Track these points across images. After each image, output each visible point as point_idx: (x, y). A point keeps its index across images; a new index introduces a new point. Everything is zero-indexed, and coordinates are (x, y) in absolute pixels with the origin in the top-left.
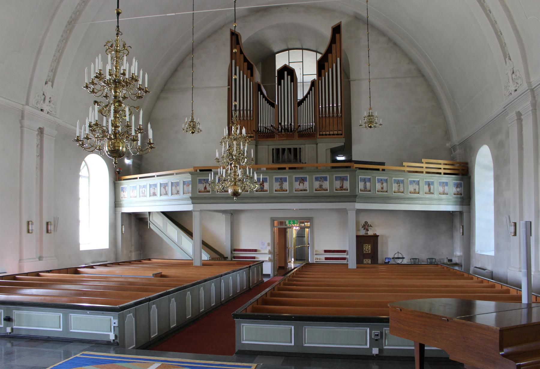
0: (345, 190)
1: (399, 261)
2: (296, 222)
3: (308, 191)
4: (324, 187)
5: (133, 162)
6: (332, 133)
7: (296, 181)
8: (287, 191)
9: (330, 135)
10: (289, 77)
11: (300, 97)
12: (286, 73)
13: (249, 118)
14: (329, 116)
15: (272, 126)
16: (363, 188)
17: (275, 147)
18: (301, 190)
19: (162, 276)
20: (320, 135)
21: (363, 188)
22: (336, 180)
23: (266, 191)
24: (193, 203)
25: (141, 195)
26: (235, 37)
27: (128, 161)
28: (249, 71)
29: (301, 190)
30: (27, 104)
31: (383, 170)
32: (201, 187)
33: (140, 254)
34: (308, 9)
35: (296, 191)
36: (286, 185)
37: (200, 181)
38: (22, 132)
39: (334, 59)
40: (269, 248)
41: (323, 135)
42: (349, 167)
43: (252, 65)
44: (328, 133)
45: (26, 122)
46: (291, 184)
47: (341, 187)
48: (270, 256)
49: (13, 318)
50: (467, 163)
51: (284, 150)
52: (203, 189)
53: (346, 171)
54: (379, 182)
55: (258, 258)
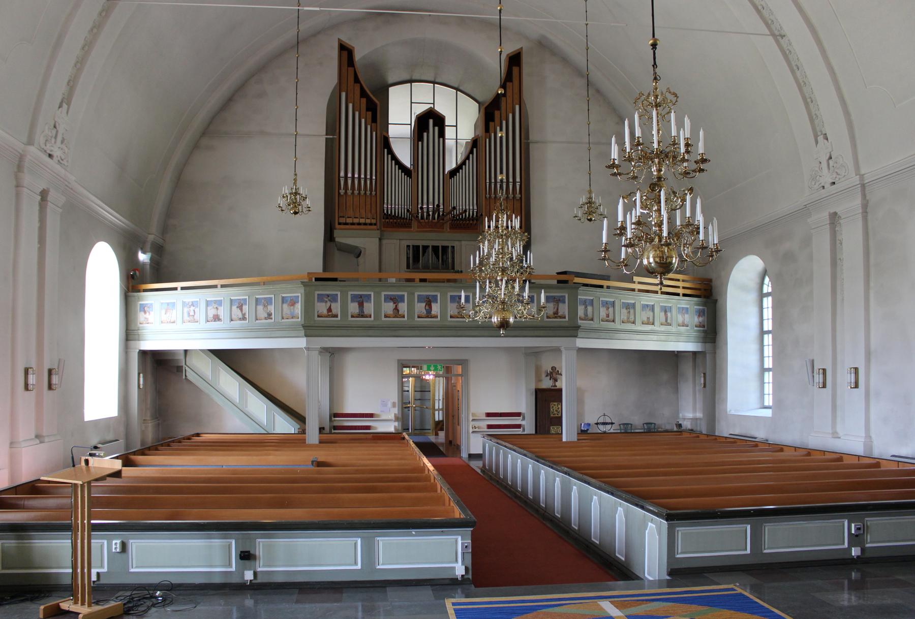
0: (561, 317)
1: (607, 428)
2: (439, 367)
5: (151, 259)
10: (436, 128)
11: (451, 165)
12: (431, 121)
13: (368, 193)
16: (583, 316)
17: (411, 243)
19: (320, 464)
20: (340, 224)
21: (583, 316)
22: (352, 301)
23: (436, 317)
24: (306, 336)
25: (186, 317)
26: (346, 52)
27: (143, 257)
28: (370, 113)
30: (30, 142)
31: (608, 287)
32: (322, 308)
33: (159, 424)
35: (319, 316)
37: (321, 298)
38: (18, 195)
40: (395, 411)
43: (376, 105)
45: (27, 179)
48: (396, 424)
49: (257, 554)
50: (710, 281)
51: (425, 248)
52: (325, 312)
54: (603, 306)
55: (375, 428)
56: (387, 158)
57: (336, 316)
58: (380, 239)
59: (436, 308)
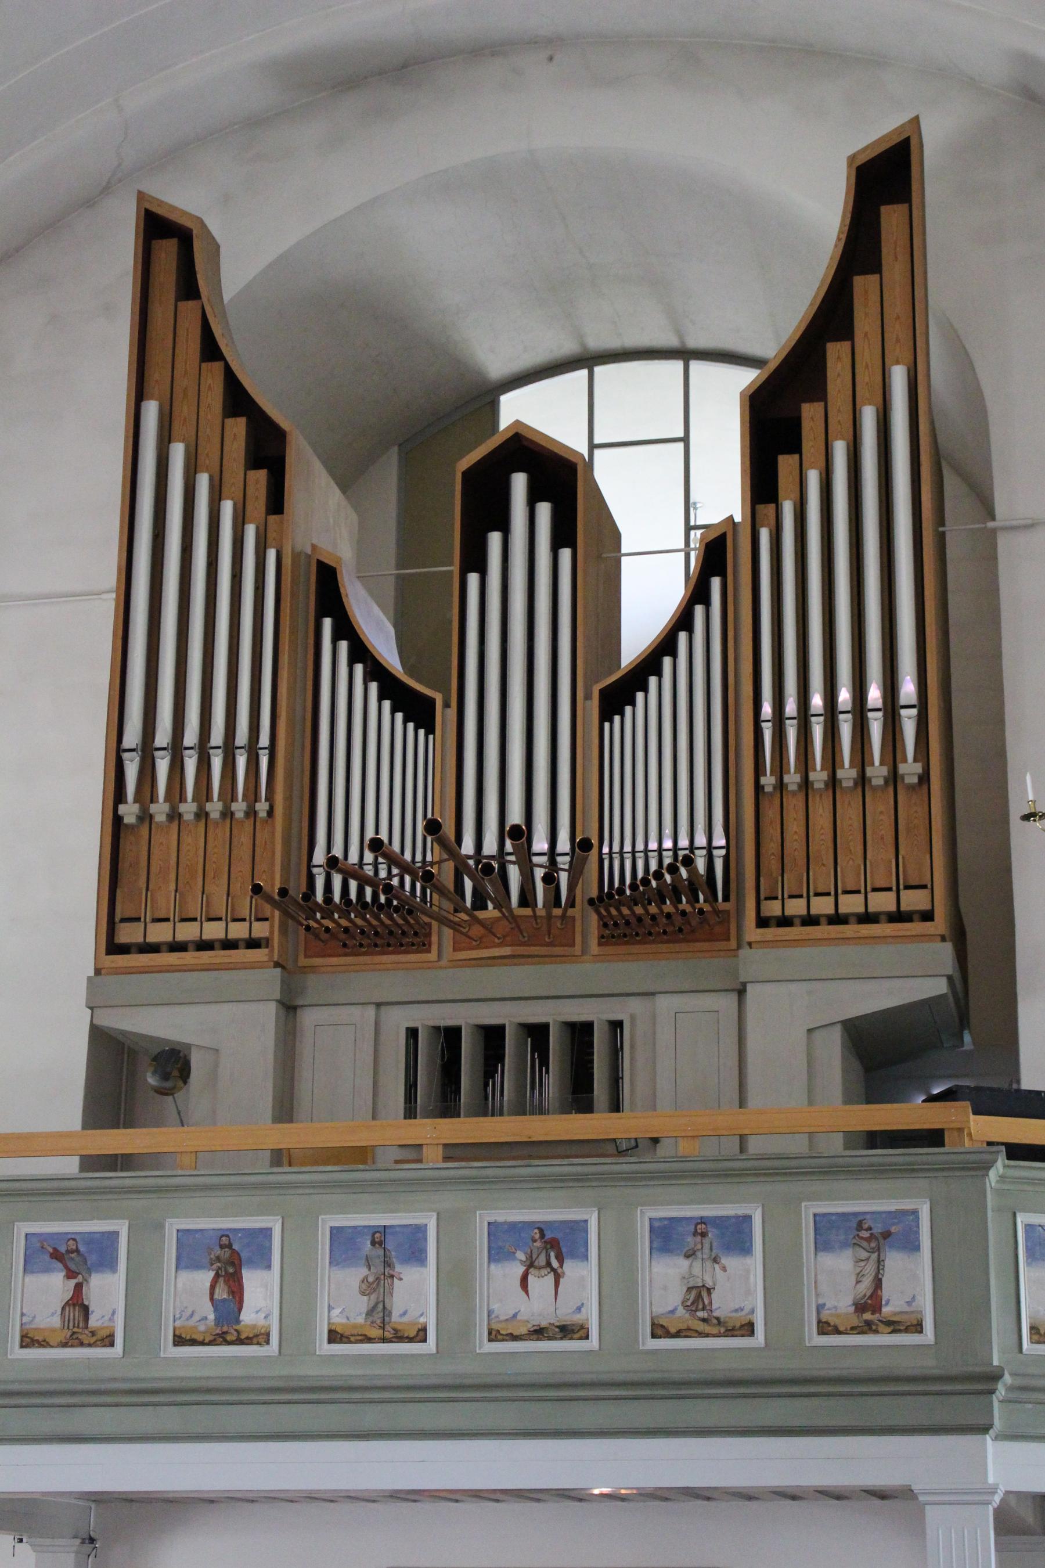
0: (894, 1326)
3: (593, 1342)
4: (723, 1304)
6: (851, 904)
7: (497, 1254)
8: (421, 1335)
9: (837, 919)
10: (544, 510)
12: (519, 482)
14: (833, 782)
15: (376, 845)
17: (426, 1017)
18: (539, 1333)
20: (763, 922)
22: (822, 1245)
23: (261, 1338)
26: (170, 246)
28: (260, 477)
29: (539, 1333)
34: (691, 56)
35: (494, 1336)
36: (416, 1293)
39: (869, 377)
41: (785, 921)
42: (934, 1138)
44: (823, 906)
46: (456, 1284)
47: (860, 1307)
51: (492, 1037)
53: (911, 1170)
56: (333, 655)
57: (109, 1341)
58: (289, 1008)
59: (261, 1296)
